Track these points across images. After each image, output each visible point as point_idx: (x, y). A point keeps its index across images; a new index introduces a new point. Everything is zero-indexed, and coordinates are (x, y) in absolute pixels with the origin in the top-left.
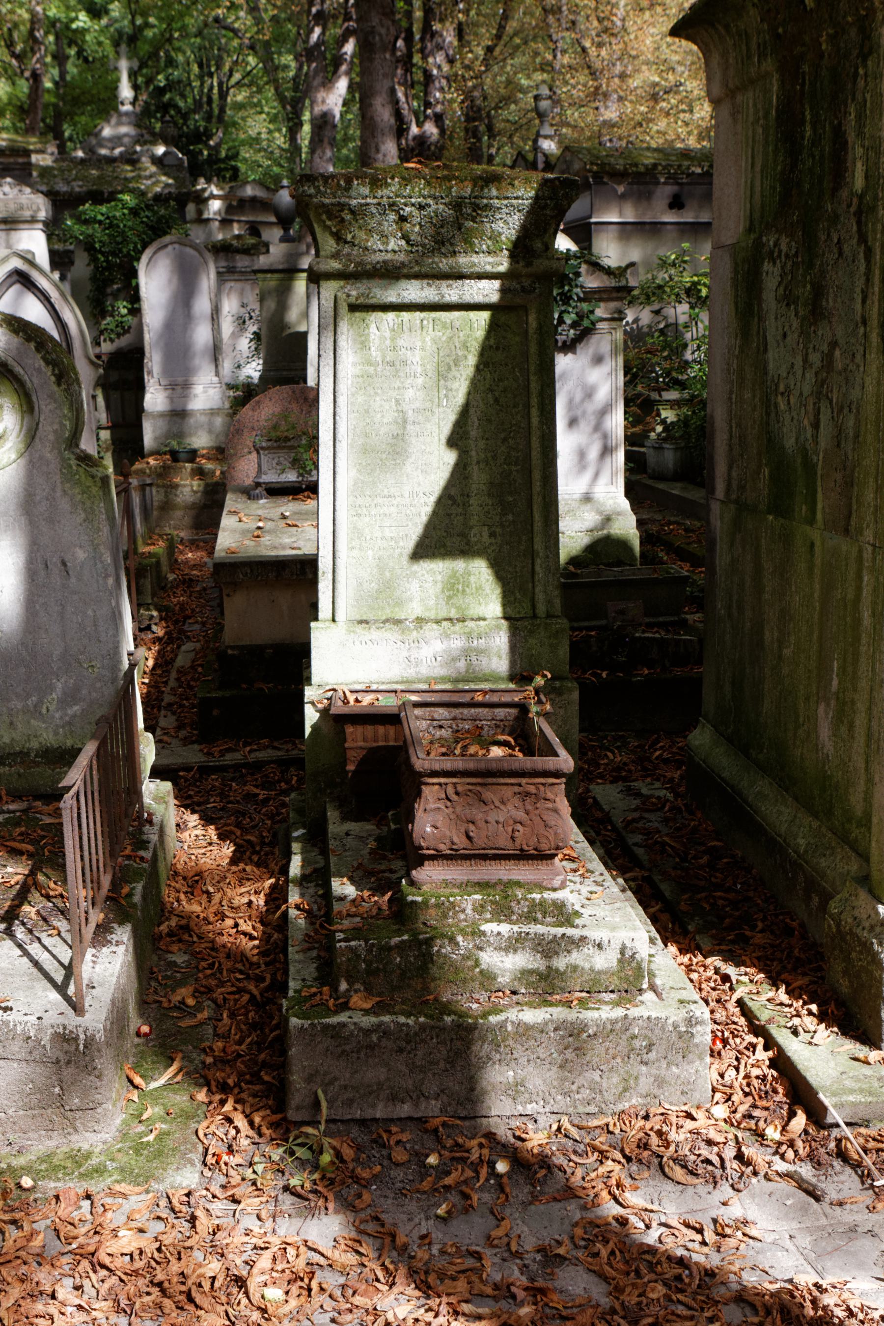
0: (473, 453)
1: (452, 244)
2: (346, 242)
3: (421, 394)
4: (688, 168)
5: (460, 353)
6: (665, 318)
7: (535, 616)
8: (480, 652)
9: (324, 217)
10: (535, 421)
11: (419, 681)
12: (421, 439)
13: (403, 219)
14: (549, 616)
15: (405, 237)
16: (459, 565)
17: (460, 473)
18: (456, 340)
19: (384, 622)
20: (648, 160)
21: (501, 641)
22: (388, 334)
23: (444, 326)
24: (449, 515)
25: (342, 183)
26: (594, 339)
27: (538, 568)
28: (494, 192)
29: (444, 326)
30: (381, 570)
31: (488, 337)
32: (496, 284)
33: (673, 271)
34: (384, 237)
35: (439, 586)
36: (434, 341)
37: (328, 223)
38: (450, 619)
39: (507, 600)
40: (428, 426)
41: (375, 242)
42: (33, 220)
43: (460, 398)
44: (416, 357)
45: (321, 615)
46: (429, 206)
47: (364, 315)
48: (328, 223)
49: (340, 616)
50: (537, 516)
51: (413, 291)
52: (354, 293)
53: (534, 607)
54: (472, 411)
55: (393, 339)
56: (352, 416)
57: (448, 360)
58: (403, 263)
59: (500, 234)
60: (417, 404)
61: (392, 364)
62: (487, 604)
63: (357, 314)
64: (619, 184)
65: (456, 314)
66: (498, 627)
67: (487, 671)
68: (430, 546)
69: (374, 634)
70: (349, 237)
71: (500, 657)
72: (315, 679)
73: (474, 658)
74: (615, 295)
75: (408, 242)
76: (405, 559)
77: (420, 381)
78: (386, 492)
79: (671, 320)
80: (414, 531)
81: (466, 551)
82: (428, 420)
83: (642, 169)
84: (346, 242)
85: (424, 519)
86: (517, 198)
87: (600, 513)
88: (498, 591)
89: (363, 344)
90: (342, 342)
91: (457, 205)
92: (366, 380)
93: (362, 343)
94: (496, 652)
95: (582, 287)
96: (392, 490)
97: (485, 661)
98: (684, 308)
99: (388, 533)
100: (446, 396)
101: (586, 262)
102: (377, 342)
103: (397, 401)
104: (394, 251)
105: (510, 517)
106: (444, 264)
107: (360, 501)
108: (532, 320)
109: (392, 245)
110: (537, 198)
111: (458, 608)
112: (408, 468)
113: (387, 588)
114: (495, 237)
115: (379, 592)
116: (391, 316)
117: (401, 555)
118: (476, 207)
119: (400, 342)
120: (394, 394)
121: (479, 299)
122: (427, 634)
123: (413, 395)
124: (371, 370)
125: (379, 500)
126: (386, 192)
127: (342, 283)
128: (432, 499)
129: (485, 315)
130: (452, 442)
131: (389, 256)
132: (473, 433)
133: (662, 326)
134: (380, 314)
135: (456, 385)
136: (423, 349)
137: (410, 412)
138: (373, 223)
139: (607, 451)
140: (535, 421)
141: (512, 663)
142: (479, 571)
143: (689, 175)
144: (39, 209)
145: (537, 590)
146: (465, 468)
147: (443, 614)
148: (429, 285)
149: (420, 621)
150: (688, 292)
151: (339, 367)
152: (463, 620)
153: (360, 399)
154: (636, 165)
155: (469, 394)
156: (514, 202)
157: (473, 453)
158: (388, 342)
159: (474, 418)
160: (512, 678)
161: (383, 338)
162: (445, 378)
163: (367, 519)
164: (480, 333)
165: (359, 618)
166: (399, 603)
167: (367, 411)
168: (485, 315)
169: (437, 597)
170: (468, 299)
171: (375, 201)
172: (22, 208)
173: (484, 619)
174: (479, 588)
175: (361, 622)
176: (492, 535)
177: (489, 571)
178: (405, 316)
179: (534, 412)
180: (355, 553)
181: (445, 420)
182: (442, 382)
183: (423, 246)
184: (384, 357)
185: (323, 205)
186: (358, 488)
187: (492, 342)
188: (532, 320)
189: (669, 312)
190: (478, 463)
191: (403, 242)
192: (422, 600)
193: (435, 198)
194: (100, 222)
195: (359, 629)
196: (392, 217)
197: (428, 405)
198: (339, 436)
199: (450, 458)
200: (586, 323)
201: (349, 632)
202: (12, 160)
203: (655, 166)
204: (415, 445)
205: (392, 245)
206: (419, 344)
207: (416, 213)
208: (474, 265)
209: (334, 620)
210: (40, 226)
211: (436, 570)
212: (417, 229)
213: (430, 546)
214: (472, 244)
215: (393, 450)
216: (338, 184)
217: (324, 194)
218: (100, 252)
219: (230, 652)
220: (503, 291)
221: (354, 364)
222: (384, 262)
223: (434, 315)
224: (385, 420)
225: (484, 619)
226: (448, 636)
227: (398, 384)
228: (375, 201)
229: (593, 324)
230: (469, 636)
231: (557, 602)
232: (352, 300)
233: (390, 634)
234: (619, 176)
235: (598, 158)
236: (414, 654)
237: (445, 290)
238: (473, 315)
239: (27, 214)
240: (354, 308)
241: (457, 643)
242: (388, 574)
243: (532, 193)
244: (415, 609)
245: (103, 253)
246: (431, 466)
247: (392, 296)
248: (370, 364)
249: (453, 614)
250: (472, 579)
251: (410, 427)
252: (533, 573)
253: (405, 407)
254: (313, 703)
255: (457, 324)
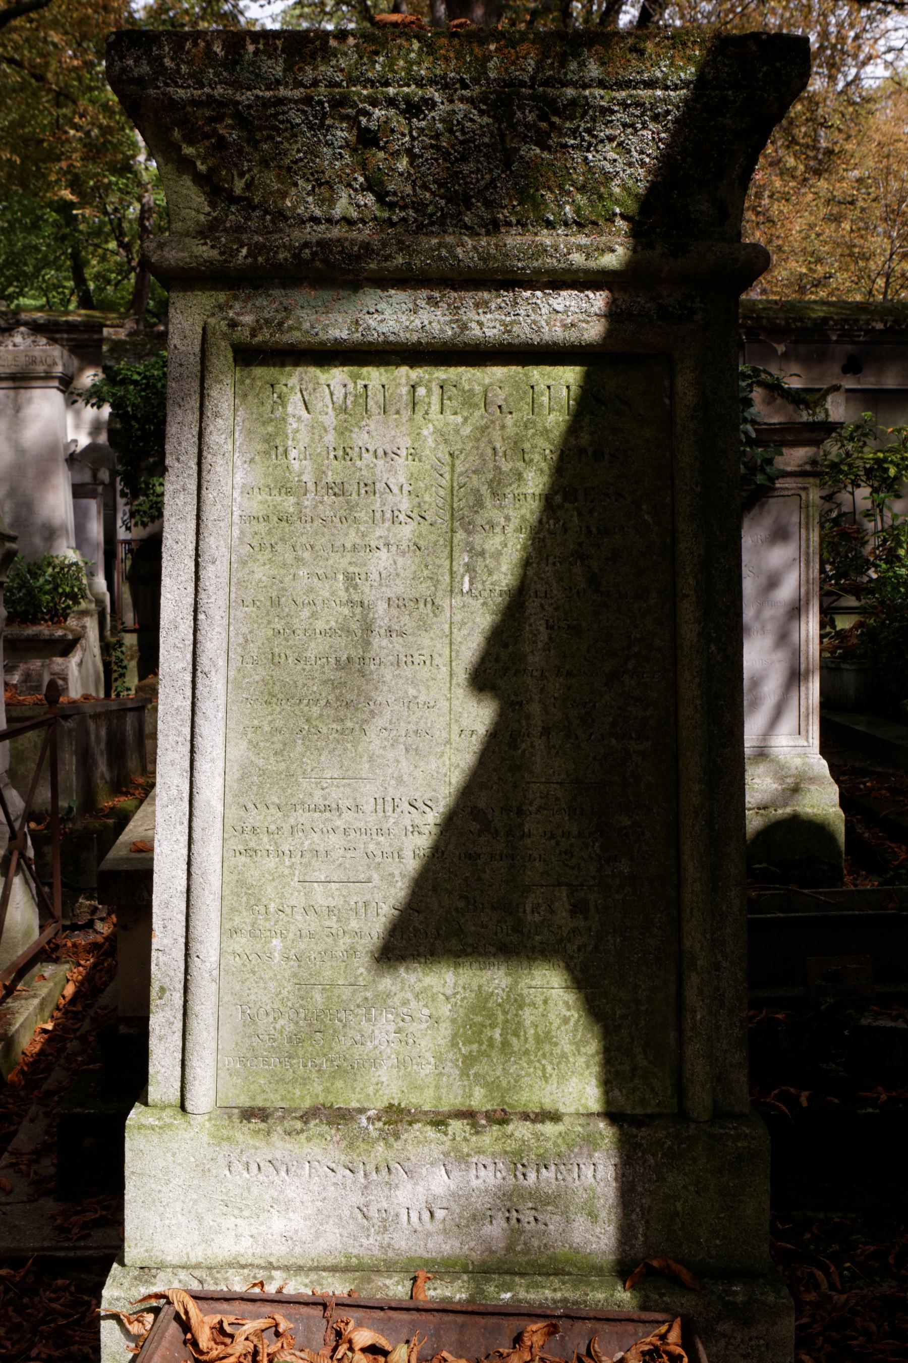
0: (535, 708)
1: (489, 204)
2: (232, 199)
3: (408, 564)
4: (867, 322)
5: (506, 466)
6: (839, 505)
7: (682, 1116)
8: (543, 1200)
9: (176, 134)
10: (689, 632)
11: (389, 1267)
12: (408, 671)
13: (368, 139)
14: (720, 1114)
15: (374, 185)
16: (496, 979)
17: (499, 756)
18: (496, 435)
19: (305, 1118)
20: (819, 313)
21: (596, 1175)
22: (330, 419)
23: (468, 400)
24: (472, 857)
25: (217, 48)
26: (774, 504)
27: (691, 996)
28: (594, 70)
29: (468, 400)
30: (304, 986)
31: (573, 428)
32: (598, 300)
33: (850, 447)
34: (324, 186)
35: (445, 1029)
36: (442, 436)
37: (188, 150)
38: (468, 1115)
39: (615, 1073)
40: (425, 640)
41: (301, 200)
42: (48, 377)
43: (504, 573)
44: (399, 473)
45: (154, 1092)
46: (431, 104)
47: (272, 372)
48: (188, 150)
49: (202, 1097)
50: (691, 869)
51: (395, 315)
52: (248, 319)
53: (680, 1091)
54: (532, 606)
55: (342, 431)
56: (239, 613)
57: (475, 481)
58: (366, 247)
59: (608, 177)
60: (399, 588)
61: (338, 490)
62: (562, 1079)
63: (258, 371)
64: (779, 343)
65: (498, 372)
66: (590, 1141)
67: (561, 1250)
68: (421, 933)
69: (280, 1146)
70: (239, 186)
71: (593, 1216)
72: (133, 1252)
73: (528, 1217)
74: (806, 436)
75: (380, 199)
76: (362, 966)
77: (407, 531)
78: (318, 798)
79: (845, 509)
80: (387, 894)
81: (511, 944)
82: (424, 626)
83: (809, 324)
84: (232, 199)
85: (411, 865)
86: (650, 84)
87: (782, 779)
88: (593, 1047)
89: (273, 444)
90: (217, 437)
91: (501, 101)
92: (276, 529)
93: (268, 439)
94: (588, 1198)
95: (754, 422)
96: (335, 794)
97: (555, 1224)
98: (864, 492)
99: (320, 897)
100: (470, 568)
101: (761, 384)
102: (304, 437)
103: (349, 578)
104: (347, 221)
105: (624, 867)
106: (467, 250)
107: (254, 818)
108: (685, 384)
109: (342, 206)
110: (700, 84)
111: (491, 1087)
112: (374, 741)
113: (314, 1030)
114: (595, 185)
115: (296, 1040)
116: (338, 376)
117: (352, 951)
118: (549, 108)
119: (360, 438)
120: (343, 562)
121: (554, 333)
122: (412, 1151)
123: (389, 564)
124: (289, 503)
125: (302, 817)
126: (325, 70)
127: (222, 297)
128: (432, 818)
129: (569, 376)
130: (483, 679)
131: (336, 232)
132: (535, 660)
133: (834, 514)
134: (314, 371)
135: (493, 543)
136: (414, 454)
137: (382, 606)
138: (295, 151)
139: (795, 677)
140: (689, 632)
141: (626, 1233)
142: (549, 994)
143: (867, 332)
144: (55, 364)
145: (689, 1051)
146: (513, 744)
147: (452, 1100)
148: (433, 303)
149: (396, 1116)
150: (869, 472)
151: (209, 496)
152: (500, 1118)
153: (260, 573)
154: (801, 320)
155: (526, 563)
156: (644, 94)
157: (535, 708)
158: (330, 438)
159: (537, 625)
160: (626, 1269)
161: (317, 428)
162: (469, 527)
163: (271, 863)
164: (556, 420)
165: (244, 1101)
166: (346, 1070)
167: (276, 603)
168: (569, 376)
169: (439, 1058)
170: (523, 332)
171: (298, 93)
172: (34, 362)
173: (555, 1117)
174: (545, 1039)
175: (249, 1114)
176: (578, 908)
177: (570, 997)
178: (374, 376)
179: (688, 610)
180: (241, 943)
181: (468, 625)
182: (460, 535)
183: (419, 207)
184: (320, 472)
185: (173, 105)
186: (248, 788)
187: (585, 439)
188: (685, 384)
189: (845, 496)
190: (546, 731)
191: (369, 199)
192: (401, 1064)
193: (444, 84)
194: (135, 383)
195: (243, 1133)
196: (342, 134)
197: (425, 589)
198: (204, 662)
199: (478, 717)
200: (760, 479)
201: (219, 1139)
202: (86, 336)
203: (825, 320)
204: (392, 686)
205: (342, 206)
206: (405, 442)
207: (399, 123)
208: (543, 251)
209: (183, 1107)
210: (56, 384)
211: (438, 990)
212: (403, 164)
213: (421, 933)
214: (538, 204)
215: (335, 691)
216: (209, 53)
217: (173, 78)
218: (134, 417)
219: (123, 1029)
220: (613, 315)
221: (247, 491)
222: (321, 243)
223: (442, 373)
224: (320, 625)
225: (555, 1117)
226: (463, 1159)
227: (353, 537)
228: (298, 93)
229: (772, 479)
230: (517, 1160)
231: (741, 1078)
232: (243, 335)
233: (319, 1149)
234: (778, 332)
235: (753, 311)
236: (378, 1201)
237: (470, 315)
238: (538, 374)
239: (40, 369)
240: (248, 356)
241: (486, 1178)
242: (318, 998)
243: (689, 73)
244: (385, 1085)
245: (137, 420)
246: (431, 739)
247: (338, 328)
248: (285, 489)
249: (479, 1099)
250: (528, 1016)
251: (379, 642)
252: (680, 1006)
253: (369, 593)
254: (116, 1317)
255: (500, 396)
